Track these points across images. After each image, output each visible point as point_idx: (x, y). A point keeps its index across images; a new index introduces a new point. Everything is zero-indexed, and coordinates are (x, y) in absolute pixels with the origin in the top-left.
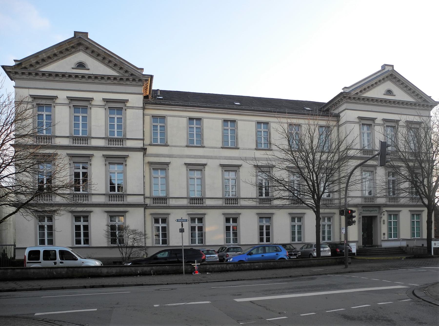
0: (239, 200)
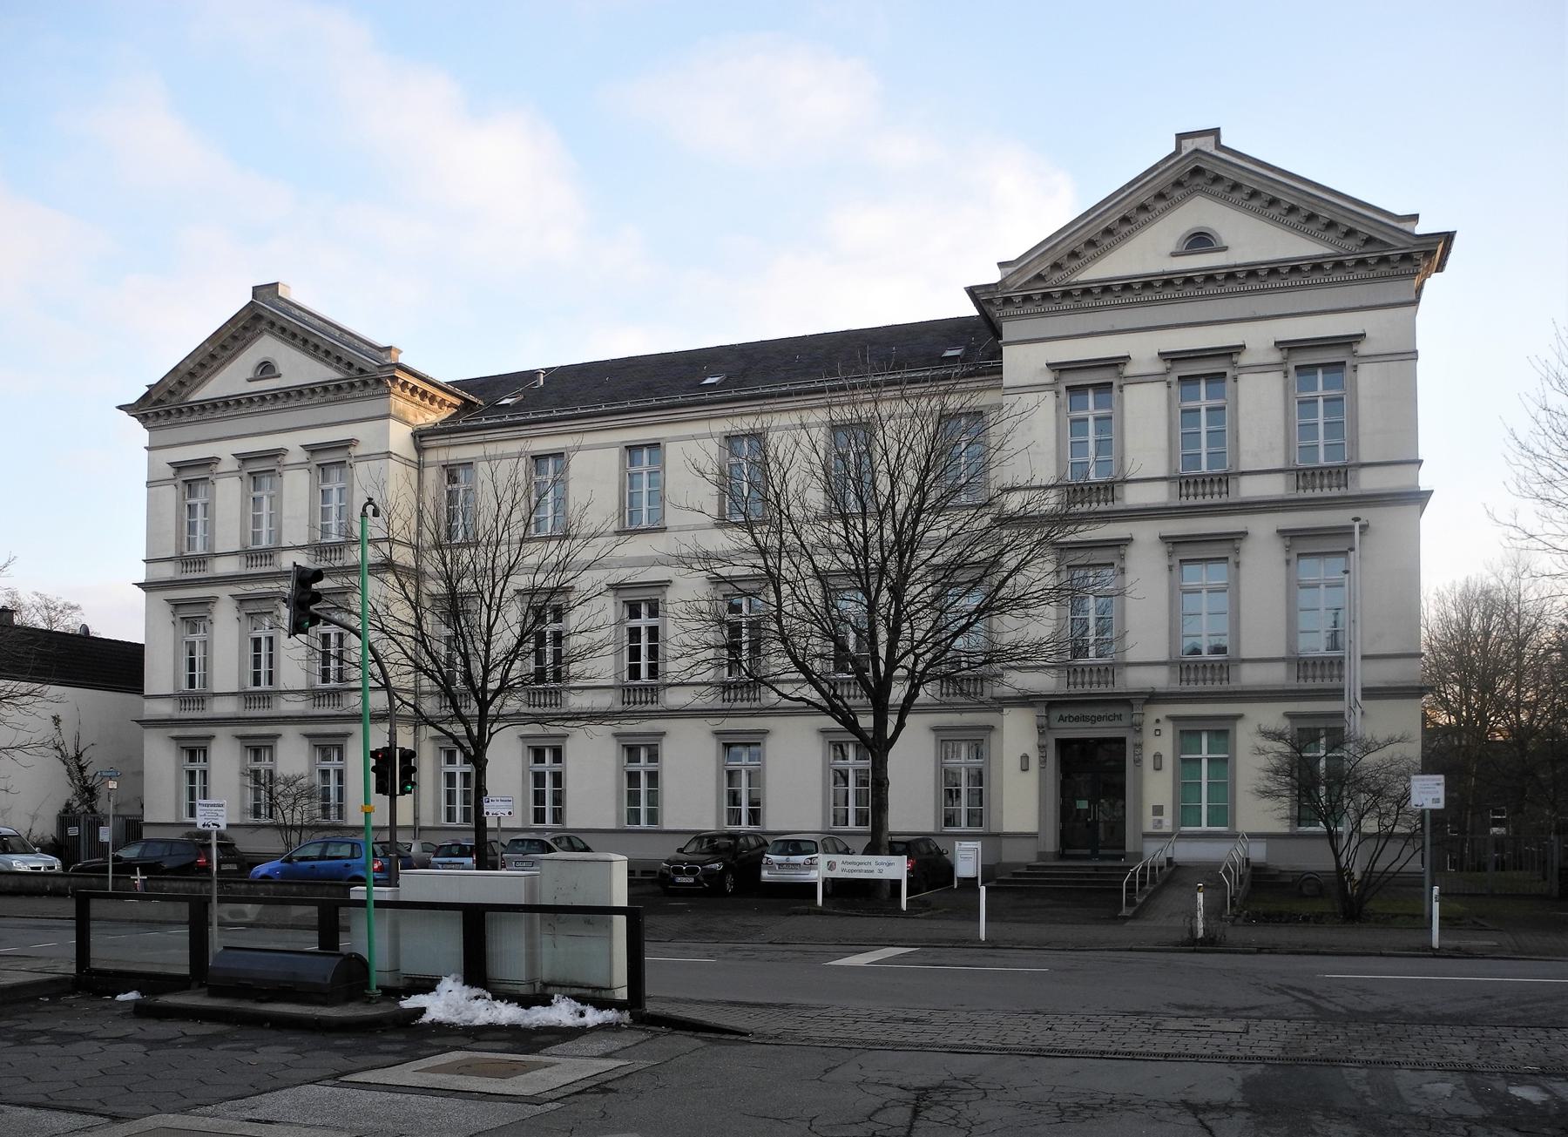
0: (564, 694)
